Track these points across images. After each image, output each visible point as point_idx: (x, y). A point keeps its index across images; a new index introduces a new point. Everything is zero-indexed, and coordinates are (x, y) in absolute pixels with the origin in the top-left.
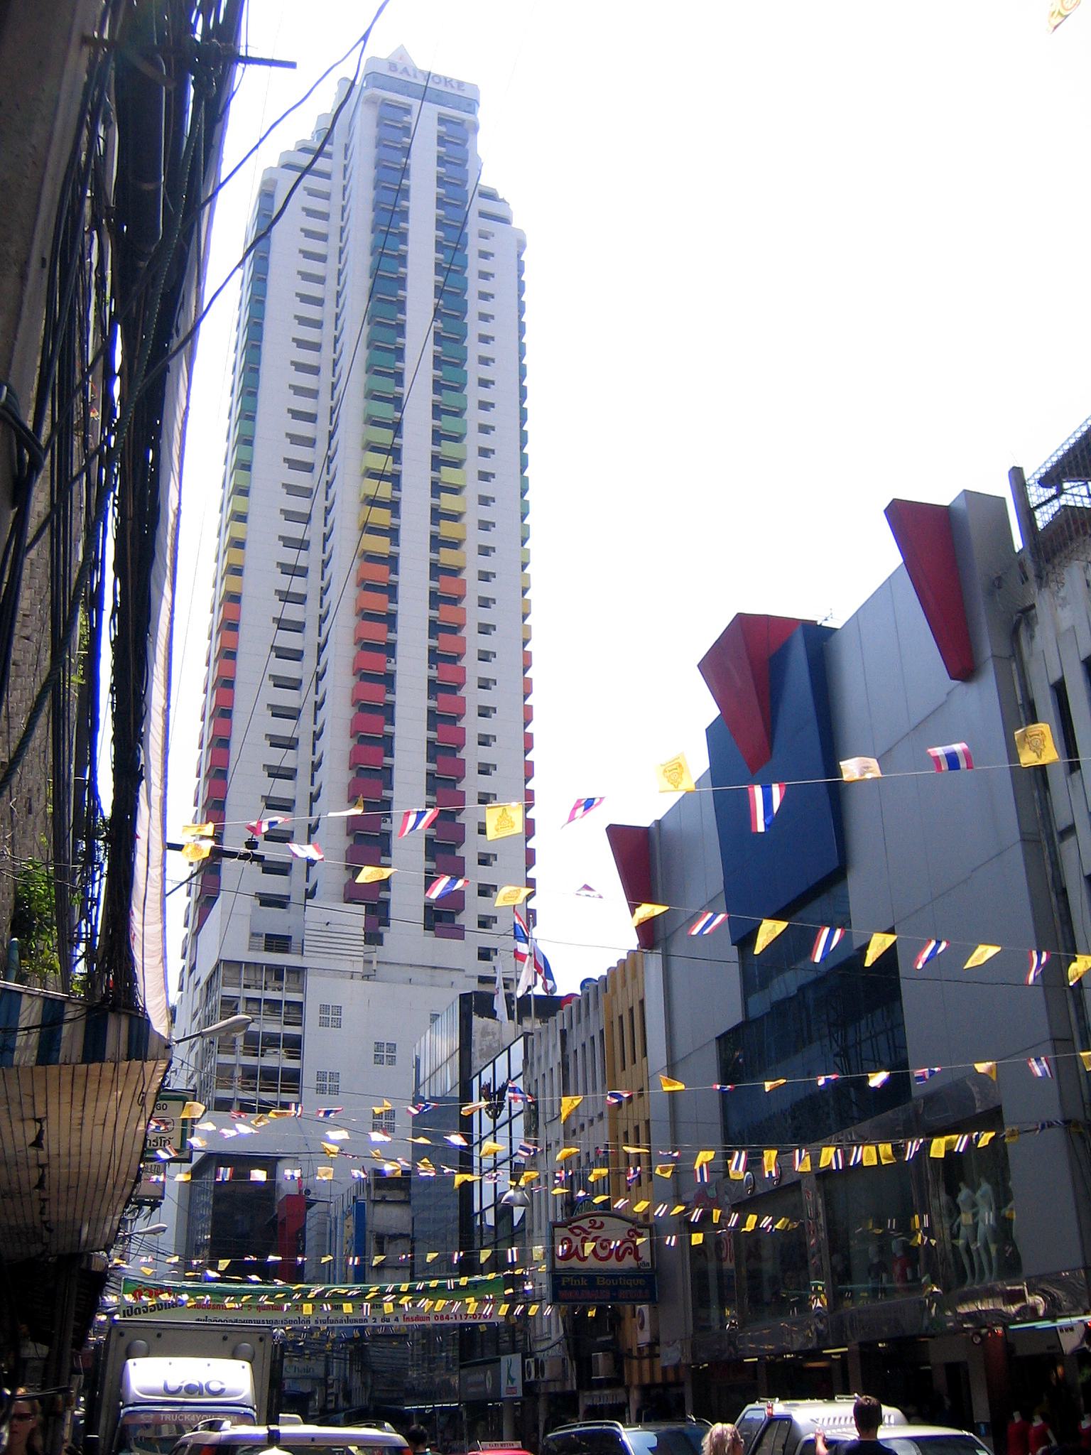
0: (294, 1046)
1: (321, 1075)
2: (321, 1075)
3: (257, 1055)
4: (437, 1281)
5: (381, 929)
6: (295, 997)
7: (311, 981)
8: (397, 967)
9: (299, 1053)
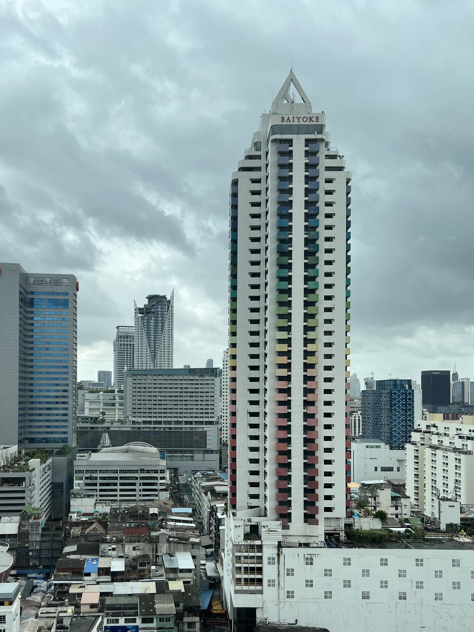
0: (260, 570)
1: (269, 581)
2: (269, 581)
3: (248, 552)
4: (20, 593)
5: (289, 524)
6: (259, 576)
7: (264, 549)
8: (294, 537)
9: (262, 573)
